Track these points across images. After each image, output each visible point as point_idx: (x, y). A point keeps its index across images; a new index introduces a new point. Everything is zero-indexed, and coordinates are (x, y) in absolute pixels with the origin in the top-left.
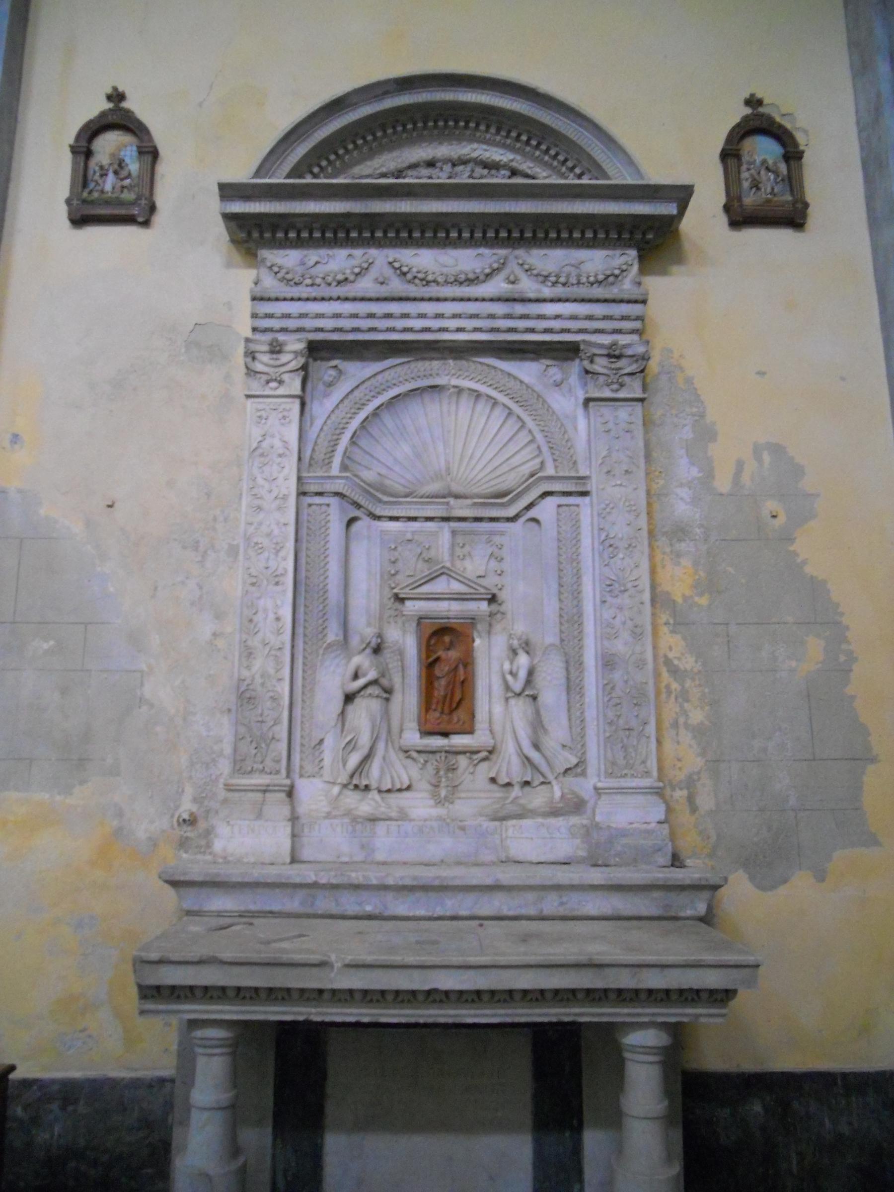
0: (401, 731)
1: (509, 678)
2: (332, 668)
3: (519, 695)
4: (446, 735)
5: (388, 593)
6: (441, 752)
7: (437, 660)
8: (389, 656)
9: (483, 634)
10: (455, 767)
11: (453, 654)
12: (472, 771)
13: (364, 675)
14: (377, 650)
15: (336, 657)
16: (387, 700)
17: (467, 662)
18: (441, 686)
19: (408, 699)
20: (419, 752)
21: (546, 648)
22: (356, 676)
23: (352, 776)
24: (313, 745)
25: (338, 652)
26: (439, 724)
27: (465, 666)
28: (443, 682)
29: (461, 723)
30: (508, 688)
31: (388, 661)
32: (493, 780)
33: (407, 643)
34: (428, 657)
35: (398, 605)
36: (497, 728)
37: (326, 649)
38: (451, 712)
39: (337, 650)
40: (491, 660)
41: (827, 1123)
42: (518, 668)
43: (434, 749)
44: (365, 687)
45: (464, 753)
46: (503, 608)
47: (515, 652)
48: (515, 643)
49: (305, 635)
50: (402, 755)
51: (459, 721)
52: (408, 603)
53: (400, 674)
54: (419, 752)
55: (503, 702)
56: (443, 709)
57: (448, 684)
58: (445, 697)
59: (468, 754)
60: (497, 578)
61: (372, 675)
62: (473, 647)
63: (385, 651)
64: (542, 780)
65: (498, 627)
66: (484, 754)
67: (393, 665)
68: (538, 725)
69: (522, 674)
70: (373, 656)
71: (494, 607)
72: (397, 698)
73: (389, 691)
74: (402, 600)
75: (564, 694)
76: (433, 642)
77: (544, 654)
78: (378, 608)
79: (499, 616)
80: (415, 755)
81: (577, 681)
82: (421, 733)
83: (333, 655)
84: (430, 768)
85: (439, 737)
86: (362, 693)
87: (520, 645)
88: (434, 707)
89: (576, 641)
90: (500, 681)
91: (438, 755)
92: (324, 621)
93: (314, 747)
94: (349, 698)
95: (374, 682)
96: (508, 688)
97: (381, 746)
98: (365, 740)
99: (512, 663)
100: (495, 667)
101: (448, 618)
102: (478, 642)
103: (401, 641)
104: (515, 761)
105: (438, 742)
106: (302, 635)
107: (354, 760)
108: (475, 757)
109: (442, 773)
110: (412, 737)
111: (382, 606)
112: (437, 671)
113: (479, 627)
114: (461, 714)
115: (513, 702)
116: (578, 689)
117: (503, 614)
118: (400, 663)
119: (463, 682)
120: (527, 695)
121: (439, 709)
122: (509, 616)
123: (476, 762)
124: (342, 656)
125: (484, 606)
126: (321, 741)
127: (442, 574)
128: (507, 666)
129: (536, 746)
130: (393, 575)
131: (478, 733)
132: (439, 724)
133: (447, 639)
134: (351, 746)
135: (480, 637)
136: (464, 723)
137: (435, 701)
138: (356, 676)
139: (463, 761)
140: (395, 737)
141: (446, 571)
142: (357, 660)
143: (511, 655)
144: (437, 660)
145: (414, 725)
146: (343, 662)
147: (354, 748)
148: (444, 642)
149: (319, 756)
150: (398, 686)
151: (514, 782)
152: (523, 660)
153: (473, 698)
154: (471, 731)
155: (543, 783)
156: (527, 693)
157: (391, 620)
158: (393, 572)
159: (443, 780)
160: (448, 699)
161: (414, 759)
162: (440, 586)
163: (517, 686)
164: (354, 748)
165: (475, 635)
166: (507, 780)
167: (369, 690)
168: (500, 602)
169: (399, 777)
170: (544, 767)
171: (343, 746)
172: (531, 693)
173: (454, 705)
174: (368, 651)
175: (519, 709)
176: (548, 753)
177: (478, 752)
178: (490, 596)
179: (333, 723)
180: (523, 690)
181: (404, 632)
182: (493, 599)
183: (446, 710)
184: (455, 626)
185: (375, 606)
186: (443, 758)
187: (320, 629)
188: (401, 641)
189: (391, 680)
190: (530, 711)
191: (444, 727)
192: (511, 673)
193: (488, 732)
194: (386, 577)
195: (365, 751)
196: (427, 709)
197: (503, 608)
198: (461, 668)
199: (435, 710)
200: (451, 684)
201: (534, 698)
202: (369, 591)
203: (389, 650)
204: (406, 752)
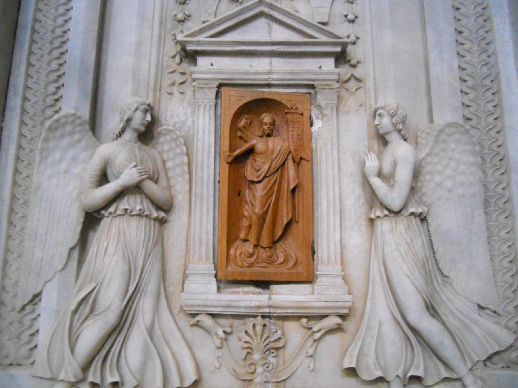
0: (185, 276)
1: (377, 182)
2: (63, 166)
3: (397, 213)
4: (263, 284)
5: (172, 49)
6: (255, 316)
7: (251, 151)
8: (166, 147)
9: (327, 112)
10: (280, 344)
11: (276, 145)
12: (311, 352)
13: (117, 177)
14: (147, 135)
15: (71, 145)
16: (162, 222)
17: (301, 157)
18: (256, 198)
19: (197, 221)
20: (213, 316)
21: (441, 131)
22: (103, 178)
23: (86, 368)
24: (19, 304)
25: (77, 137)
26: (250, 265)
27: (298, 163)
28: (260, 190)
29: (291, 264)
30: (373, 198)
31: (165, 156)
32: (352, 372)
33: (196, 125)
34: (232, 149)
35: (186, 66)
36: (356, 273)
37: (51, 129)
38: (274, 243)
39: (71, 133)
40: (339, 150)
41: (261, 160)
42: (395, 164)
43: (242, 311)
44: (118, 196)
45: (299, 318)
46: (358, 72)
47: (383, 140)
48: (386, 122)
49: (23, 111)
50: (185, 322)
51: (286, 261)
52: (203, 62)
53: (187, 177)
54: (213, 316)
55: (364, 224)
56: (258, 239)
57: (268, 195)
58: (262, 218)
59: (304, 321)
60: (347, 25)
61: (128, 176)
62: (311, 133)
63: (162, 139)
64: (445, 374)
65: (351, 102)
66: (333, 321)
67: (176, 163)
68: (433, 269)
69: (404, 175)
70: (137, 147)
71: (345, 71)
72: (178, 221)
73: (165, 207)
74: (190, 56)
75: (479, 212)
76: (242, 123)
77: (437, 141)
78: (153, 70)
79: (353, 84)
80: (207, 321)
81: (499, 189)
82: (219, 281)
83: (65, 142)
84: (236, 344)
85: (252, 289)
86: (112, 209)
87: (395, 125)
88: (242, 235)
89: (491, 119)
90: (358, 191)
91: (250, 322)
92: (58, 88)
93: (23, 309)
94: (92, 219)
95: (136, 189)
96: (373, 198)
97: (145, 306)
98: (111, 300)
99: (380, 156)
100: (350, 167)
101: (269, 86)
102: (318, 124)
103: (189, 123)
104: (392, 334)
105: (249, 298)
106: (18, 110)
107: (91, 334)
108: (317, 326)
109: (256, 356)
110: (203, 289)
111: (160, 66)
112: (250, 173)
113: (321, 99)
114: (290, 247)
115: (384, 226)
116: (500, 204)
117: (358, 80)
118: (186, 159)
119: (293, 191)
120: (412, 214)
121: (252, 238)
122: (369, 84)
123: (318, 335)
124: (83, 144)
125: (329, 64)
126: (37, 297)
127: (261, 14)
128: (372, 163)
129: (431, 309)
130: (182, 21)
131: (321, 282)
132: (250, 265)
133: (267, 118)
134: (87, 306)
135: (323, 116)
136: (295, 264)
137: (245, 223)
138: (103, 178)
139: (294, 332)
140: (173, 288)
141: (266, 10)
142: (107, 149)
143: (375, 145)
144: (251, 151)
145: (208, 267)
146: (84, 155)
147: (92, 311)
148: (262, 123)
149: (31, 326)
150: (181, 199)
151: (390, 377)
152: (401, 151)
153: (311, 220)
154: (309, 279)
155: (446, 379)
156: (411, 210)
157: (175, 90)
158: (180, 16)
159: (260, 370)
160: (268, 218)
161: (206, 330)
162: (258, 32)
163: (394, 197)
164: (92, 311)
165: (314, 113)
166: (379, 374)
167: (124, 204)
168: (353, 62)
169: (178, 365)
170: (449, 352)
171: (73, 306)
172: (420, 210)
173: (279, 233)
174: (129, 135)
175: (396, 238)
176: (450, 320)
177: (324, 317)
178: (338, 49)
179: (59, 264)
180: (404, 207)
181: (195, 106)
182: (341, 58)
183: (265, 242)
184: (277, 98)
185: (148, 68)
186: (259, 328)
187: (50, 100)
188: (189, 123)
189: (169, 187)
190: (420, 243)
191: (259, 271)
192: (380, 174)
193: (340, 280)
194: (169, 25)
195: (110, 318)
196: (231, 238)
197: (358, 72)
198: (290, 164)
199: (246, 240)
200: (273, 195)
201: (423, 219)
202: (140, 44)
203: (168, 137)
204: (194, 315)
